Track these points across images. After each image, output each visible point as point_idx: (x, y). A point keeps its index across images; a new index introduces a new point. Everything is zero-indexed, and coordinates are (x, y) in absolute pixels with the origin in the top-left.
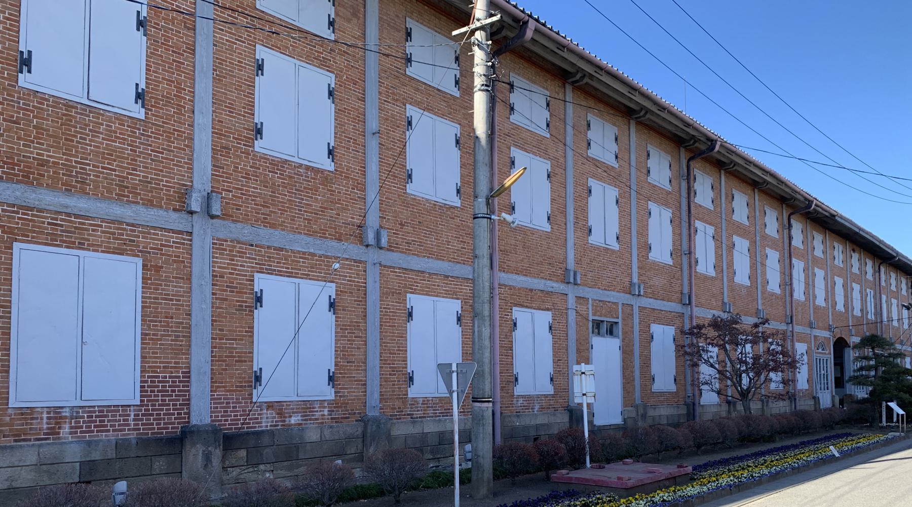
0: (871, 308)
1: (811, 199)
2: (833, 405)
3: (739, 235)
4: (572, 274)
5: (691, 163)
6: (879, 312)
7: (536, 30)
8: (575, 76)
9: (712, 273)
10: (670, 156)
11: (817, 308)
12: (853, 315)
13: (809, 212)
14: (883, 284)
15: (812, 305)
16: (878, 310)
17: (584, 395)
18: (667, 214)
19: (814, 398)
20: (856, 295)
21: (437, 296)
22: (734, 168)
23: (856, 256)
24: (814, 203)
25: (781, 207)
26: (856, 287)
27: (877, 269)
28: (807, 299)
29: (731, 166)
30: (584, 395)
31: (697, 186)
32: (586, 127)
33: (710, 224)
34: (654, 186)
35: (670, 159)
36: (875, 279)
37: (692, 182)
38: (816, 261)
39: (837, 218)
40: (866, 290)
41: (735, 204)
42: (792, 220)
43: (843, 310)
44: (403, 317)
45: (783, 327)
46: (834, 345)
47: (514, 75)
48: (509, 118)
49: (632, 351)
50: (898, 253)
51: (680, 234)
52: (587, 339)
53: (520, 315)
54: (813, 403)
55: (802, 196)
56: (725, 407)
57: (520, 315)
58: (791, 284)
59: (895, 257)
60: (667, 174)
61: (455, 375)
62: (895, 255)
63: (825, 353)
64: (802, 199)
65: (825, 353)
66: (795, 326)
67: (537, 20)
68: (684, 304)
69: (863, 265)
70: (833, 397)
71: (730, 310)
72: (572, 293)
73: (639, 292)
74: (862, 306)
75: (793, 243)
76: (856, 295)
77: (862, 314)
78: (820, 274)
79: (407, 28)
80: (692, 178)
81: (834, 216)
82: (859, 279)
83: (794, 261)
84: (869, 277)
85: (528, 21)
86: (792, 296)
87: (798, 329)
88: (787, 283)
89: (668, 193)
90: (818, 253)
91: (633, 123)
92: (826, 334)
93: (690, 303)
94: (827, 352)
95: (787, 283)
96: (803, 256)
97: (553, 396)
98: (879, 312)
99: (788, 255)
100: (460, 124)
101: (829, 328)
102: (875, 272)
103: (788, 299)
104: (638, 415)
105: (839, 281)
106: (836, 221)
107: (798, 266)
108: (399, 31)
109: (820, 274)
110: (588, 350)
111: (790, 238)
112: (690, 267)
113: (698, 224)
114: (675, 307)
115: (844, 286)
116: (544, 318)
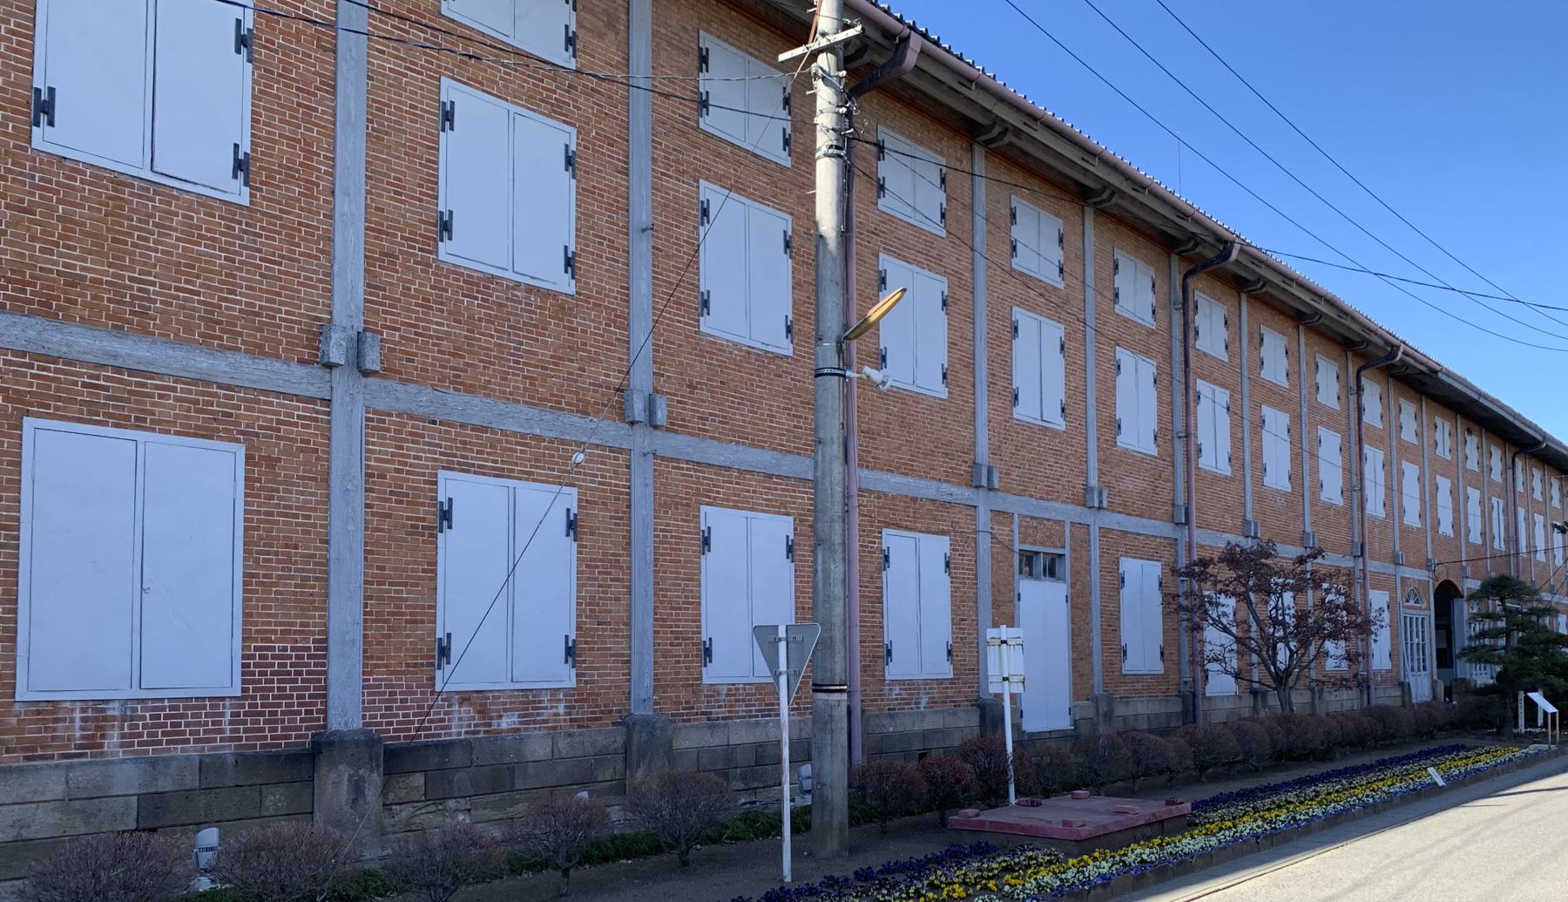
0: (1498, 529)
1: (1396, 342)
2: (1435, 697)
3: (1272, 405)
4: (984, 471)
5: (1190, 281)
6: (1512, 538)
7: (923, 53)
8: (990, 132)
9: (1225, 469)
10: (1153, 269)
11: (1406, 531)
12: (1468, 542)
13: (1393, 365)
14: (1520, 488)
15: (1397, 525)
16: (1512, 534)
17: (1005, 679)
18: (1148, 369)
19: (1401, 685)
20: (1474, 508)
21: (752, 510)
22: (1264, 290)
23: (1472, 441)
24: (1402, 350)
25: (1078, 219)
26: (1474, 494)
27: (1509, 462)
28: (1390, 515)
29: (1259, 286)
30: (1005, 679)
31: (1200, 321)
32: (1008, 219)
33: (1222, 386)
34: (1126, 320)
35: (1153, 273)
36: (1506, 480)
37: (1191, 313)
38: (1405, 450)
39: (1440, 375)
40: (1490, 499)
41: (1266, 351)
42: (1363, 378)
43: (1451, 533)
44: (694, 545)
45: (1348, 563)
46: (1435, 594)
47: (1119, 251)
48: (877, 204)
49: (1087, 605)
50: (1545, 436)
51: (1171, 403)
52: (1011, 584)
53: (895, 541)
54: (1399, 693)
55: (1381, 337)
56: (1248, 701)
57: (895, 541)
58: (1362, 489)
59: (1540, 443)
60: (1148, 299)
61: (782, 646)
62: (1540, 438)
63: (1420, 608)
64: (1381, 342)
65: (1420, 608)
66: (1196, 532)
67: (925, 36)
68: (1177, 524)
69: (1485, 455)
70: (1434, 683)
71: (1256, 533)
72: (985, 505)
73: (1101, 502)
74: (1484, 526)
75: (1366, 418)
76: (1474, 508)
77: (1484, 540)
78: (1411, 471)
79: (700, 49)
80: (1191, 306)
81: (1436, 372)
82: (1451, 470)
83: (1367, 448)
84: (1497, 476)
85: (909, 36)
86: (1362, 508)
87: (1373, 566)
88: (1355, 487)
89: (1150, 333)
90: (1409, 435)
91: (1089, 211)
92: (1421, 575)
93: (1187, 522)
94: (1424, 606)
95: (1355, 487)
96: (1381, 441)
97: (952, 681)
98: (1512, 538)
99: (1356, 440)
100: (791, 214)
101: (1428, 568)
102: (1506, 468)
103: (1356, 514)
104: (1098, 714)
105: (1444, 484)
106: (1439, 380)
107: (1374, 457)
108: (686, 53)
109: (1411, 471)
110: (1012, 601)
111: (1360, 410)
112: (1188, 459)
113: (1202, 386)
114: (1159, 528)
115: (1454, 492)
116: (937, 547)
